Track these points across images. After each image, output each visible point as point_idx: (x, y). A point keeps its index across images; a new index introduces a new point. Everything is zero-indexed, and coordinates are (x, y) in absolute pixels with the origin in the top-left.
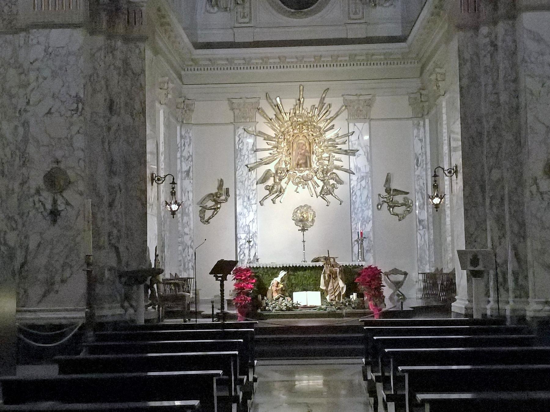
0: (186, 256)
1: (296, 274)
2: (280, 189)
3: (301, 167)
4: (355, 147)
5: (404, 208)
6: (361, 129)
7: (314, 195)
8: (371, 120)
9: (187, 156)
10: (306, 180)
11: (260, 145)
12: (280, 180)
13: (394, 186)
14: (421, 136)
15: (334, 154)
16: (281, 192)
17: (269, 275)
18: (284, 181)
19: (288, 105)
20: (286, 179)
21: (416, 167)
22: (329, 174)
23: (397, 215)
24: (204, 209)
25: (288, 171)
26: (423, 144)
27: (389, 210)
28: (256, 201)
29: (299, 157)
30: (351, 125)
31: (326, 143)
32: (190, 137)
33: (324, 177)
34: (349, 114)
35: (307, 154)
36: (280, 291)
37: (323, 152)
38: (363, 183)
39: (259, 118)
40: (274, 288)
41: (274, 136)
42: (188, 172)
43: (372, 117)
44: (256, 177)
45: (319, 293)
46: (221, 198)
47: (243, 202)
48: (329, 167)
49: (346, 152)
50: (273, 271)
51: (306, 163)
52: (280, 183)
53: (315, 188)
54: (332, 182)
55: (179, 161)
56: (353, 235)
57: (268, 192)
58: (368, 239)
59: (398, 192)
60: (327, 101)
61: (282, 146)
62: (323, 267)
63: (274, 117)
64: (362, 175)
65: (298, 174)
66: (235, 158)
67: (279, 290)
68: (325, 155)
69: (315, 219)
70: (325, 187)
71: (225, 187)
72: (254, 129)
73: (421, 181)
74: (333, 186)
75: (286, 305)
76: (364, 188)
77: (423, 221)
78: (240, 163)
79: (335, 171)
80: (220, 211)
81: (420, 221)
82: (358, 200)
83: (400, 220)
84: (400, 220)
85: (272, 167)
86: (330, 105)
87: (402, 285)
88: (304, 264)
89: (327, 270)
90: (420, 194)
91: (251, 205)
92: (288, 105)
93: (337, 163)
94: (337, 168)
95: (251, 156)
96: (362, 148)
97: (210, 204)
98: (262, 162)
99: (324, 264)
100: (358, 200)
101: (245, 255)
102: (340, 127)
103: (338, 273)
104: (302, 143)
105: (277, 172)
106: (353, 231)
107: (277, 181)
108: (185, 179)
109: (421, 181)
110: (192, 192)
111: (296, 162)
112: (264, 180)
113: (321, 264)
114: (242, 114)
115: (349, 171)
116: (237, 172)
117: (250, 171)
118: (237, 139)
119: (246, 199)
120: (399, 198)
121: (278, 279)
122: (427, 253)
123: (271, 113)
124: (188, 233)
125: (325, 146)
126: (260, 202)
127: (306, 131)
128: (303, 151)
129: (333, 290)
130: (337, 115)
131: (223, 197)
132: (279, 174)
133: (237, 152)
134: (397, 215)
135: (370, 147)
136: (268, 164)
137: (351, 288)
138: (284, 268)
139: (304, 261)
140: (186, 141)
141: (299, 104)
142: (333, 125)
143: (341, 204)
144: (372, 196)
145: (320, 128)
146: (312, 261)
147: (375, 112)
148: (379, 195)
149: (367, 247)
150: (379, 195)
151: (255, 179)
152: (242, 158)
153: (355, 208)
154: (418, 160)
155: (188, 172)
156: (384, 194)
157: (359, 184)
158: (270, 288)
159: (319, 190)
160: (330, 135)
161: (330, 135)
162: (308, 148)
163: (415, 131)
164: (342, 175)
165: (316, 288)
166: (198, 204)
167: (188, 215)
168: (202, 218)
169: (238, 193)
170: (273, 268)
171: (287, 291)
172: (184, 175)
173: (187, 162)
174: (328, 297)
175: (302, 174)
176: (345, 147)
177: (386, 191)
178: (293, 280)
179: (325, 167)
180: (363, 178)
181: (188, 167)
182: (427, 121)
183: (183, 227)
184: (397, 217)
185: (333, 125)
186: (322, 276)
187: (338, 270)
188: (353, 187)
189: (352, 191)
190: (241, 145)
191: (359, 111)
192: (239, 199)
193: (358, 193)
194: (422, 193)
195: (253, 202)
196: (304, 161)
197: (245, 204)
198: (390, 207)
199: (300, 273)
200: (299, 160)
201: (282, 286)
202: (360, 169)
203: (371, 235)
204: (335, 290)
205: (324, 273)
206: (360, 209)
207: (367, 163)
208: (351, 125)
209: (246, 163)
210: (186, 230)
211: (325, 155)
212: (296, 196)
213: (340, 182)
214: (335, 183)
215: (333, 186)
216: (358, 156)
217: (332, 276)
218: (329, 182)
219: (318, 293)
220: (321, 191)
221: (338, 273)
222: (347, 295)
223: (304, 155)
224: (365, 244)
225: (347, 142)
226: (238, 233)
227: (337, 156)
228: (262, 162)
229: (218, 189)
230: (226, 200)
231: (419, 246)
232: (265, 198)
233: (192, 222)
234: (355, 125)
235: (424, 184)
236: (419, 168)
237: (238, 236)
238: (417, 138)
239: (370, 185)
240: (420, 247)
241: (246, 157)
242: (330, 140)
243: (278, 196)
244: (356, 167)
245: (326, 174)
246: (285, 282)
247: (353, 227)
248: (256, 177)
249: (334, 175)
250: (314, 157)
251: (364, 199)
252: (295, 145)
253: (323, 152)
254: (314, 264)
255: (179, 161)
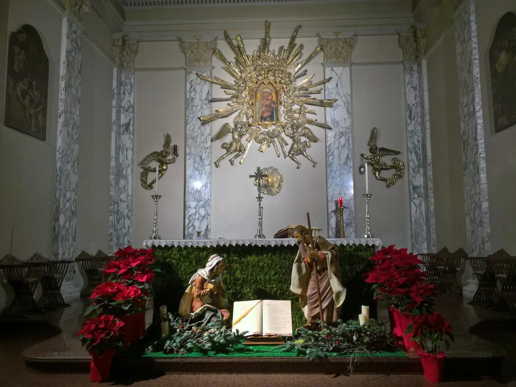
0: (121, 229)
1: (243, 259)
2: (240, 147)
3: (265, 120)
4: (333, 96)
5: (393, 171)
6: (339, 75)
7: (282, 155)
8: (352, 64)
9: (127, 107)
10: (271, 137)
11: (217, 93)
12: (241, 136)
13: (380, 144)
14: (416, 82)
15: (306, 106)
16: (241, 150)
17: (191, 263)
18: (244, 138)
19: (251, 47)
20: (248, 135)
21: (409, 121)
22: (300, 130)
23: (385, 180)
24: (147, 171)
25: (250, 125)
26: (418, 92)
27: (375, 174)
28: (211, 161)
29: (263, 109)
30: (328, 70)
31: (296, 93)
32: (131, 84)
33: (294, 133)
34: (326, 57)
35: (273, 105)
36: (207, 297)
37: (293, 102)
38: (343, 140)
39: (216, 61)
40: (195, 291)
41: (234, 83)
42: (127, 125)
43: (353, 61)
44: (211, 132)
45: (288, 303)
46: (168, 158)
47: (194, 162)
48: (300, 121)
49: (322, 104)
50: (198, 256)
51: (271, 115)
52: (240, 140)
53: (282, 147)
54: (303, 139)
55: (114, 110)
56: (330, 204)
57: (225, 151)
58: (348, 210)
59: (385, 151)
60: (298, 41)
61: (244, 95)
62: (296, 247)
63: (234, 61)
64: (341, 130)
65: (263, 130)
66: (186, 109)
67: (204, 295)
68: (296, 107)
69: (282, 184)
70: (296, 146)
71: (172, 145)
72: (209, 74)
73: (415, 139)
74: (305, 145)
75: (211, 339)
76: (344, 146)
77: (418, 187)
78: (191, 116)
79: (307, 125)
80: (166, 174)
81: (415, 188)
82: (336, 160)
83: (388, 186)
84: (388, 186)
85: (230, 121)
86: (302, 46)
87: (276, 235)
88: (260, 242)
89: (305, 254)
90: (413, 154)
91: (203, 166)
92: (251, 47)
93: (309, 116)
94: (310, 122)
95: (205, 107)
96: (341, 98)
97: (155, 165)
98: (218, 116)
99: (299, 242)
100: (336, 160)
101: (194, 228)
102: (315, 71)
103: (329, 260)
104: (267, 92)
105: (236, 126)
106: (329, 199)
107: (236, 137)
108: (123, 134)
109: (415, 139)
110: (132, 149)
111: (260, 115)
112: (220, 135)
113: (292, 241)
114: (195, 55)
115: (325, 127)
116: (188, 126)
117: (203, 124)
118: (188, 86)
119: (198, 159)
120: (387, 160)
121: (204, 272)
122: (424, 227)
123: (230, 56)
124: (125, 199)
125: (296, 96)
126: (215, 163)
127: (272, 78)
128: (269, 102)
129: (317, 297)
130: (310, 58)
131: (170, 157)
132: (240, 129)
133: (188, 103)
134: (385, 180)
135: (351, 96)
136: (225, 117)
137: (358, 293)
138: (219, 250)
139: (260, 236)
140: (126, 88)
141: (265, 45)
142: (306, 71)
143: (314, 166)
144: (353, 155)
145: (290, 74)
146: (277, 236)
147: (355, 58)
148: (362, 155)
149: (347, 219)
150: (362, 155)
151: (209, 135)
152: (194, 109)
153: (331, 171)
154: (411, 112)
155: (127, 125)
156: (368, 154)
157: (337, 142)
158: (187, 291)
159: (287, 149)
160: (302, 82)
161: (302, 82)
162: (274, 99)
163: (408, 77)
164: (316, 131)
165: (282, 294)
166: (139, 165)
167: (125, 178)
168: (144, 182)
169: (188, 151)
170: (198, 248)
171: (225, 295)
172: (122, 129)
173: (126, 114)
174: (306, 310)
175: (266, 130)
176: (319, 97)
177: (371, 150)
178: (238, 272)
179: (295, 121)
180: (342, 134)
181: (128, 119)
182: (424, 62)
183: (119, 191)
184: (384, 183)
185: (306, 71)
186: (295, 266)
187: (329, 256)
188: (330, 146)
189: (328, 150)
190: (193, 93)
191: (338, 51)
192: (189, 159)
193: (336, 153)
194: (416, 153)
195: (207, 162)
196: (269, 114)
197: (196, 165)
198: (375, 169)
199: (252, 259)
200: (263, 112)
201: (210, 286)
202: (338, 123)
203: (352, 202)
204: (321, 296)
205: (299, 261)
206: (338, 173)
207: (346, 116)
208: (328, 70)
209: (199, 115)
210: (123, 196)
211: (296, 107)
212: (258, 154)
213: (315, 140)
214: (308, 140)
215: (305, 145)
216: (336, 108)
217: (317, 266)
218: (300, 139)
219: (285, 306)
220: (290, 150)
221: (329, 260)
222: (349, 312)
223: (270, 106)
224: (345, 216)
225: (322, 91)
226: (187, 199)
227: (310, 108)
228: (218, 116)
229: (164, 147)
230: (173, 161)
231: (413, 220)
232: (222, 158)
233: (130, 187)
234: (333, 70)
235: (419, 141)
236: (413, 122)
237: (187, 204)
238: (409, 85)
239: (351, 142)
240: (415, 220)
241: (199, 108)
242: (301, 88)
243: (237, 156)
244: (334, 121)
245: (297, 129)
246: (220, 278)
247: (330, 195)
248: (211, 132)
249: (306, 131)
250: (282, 109)
251: (343, 160)
252: (259, 95)
253: (293, 102)
254: (279, 241)
255: (114, 110)
